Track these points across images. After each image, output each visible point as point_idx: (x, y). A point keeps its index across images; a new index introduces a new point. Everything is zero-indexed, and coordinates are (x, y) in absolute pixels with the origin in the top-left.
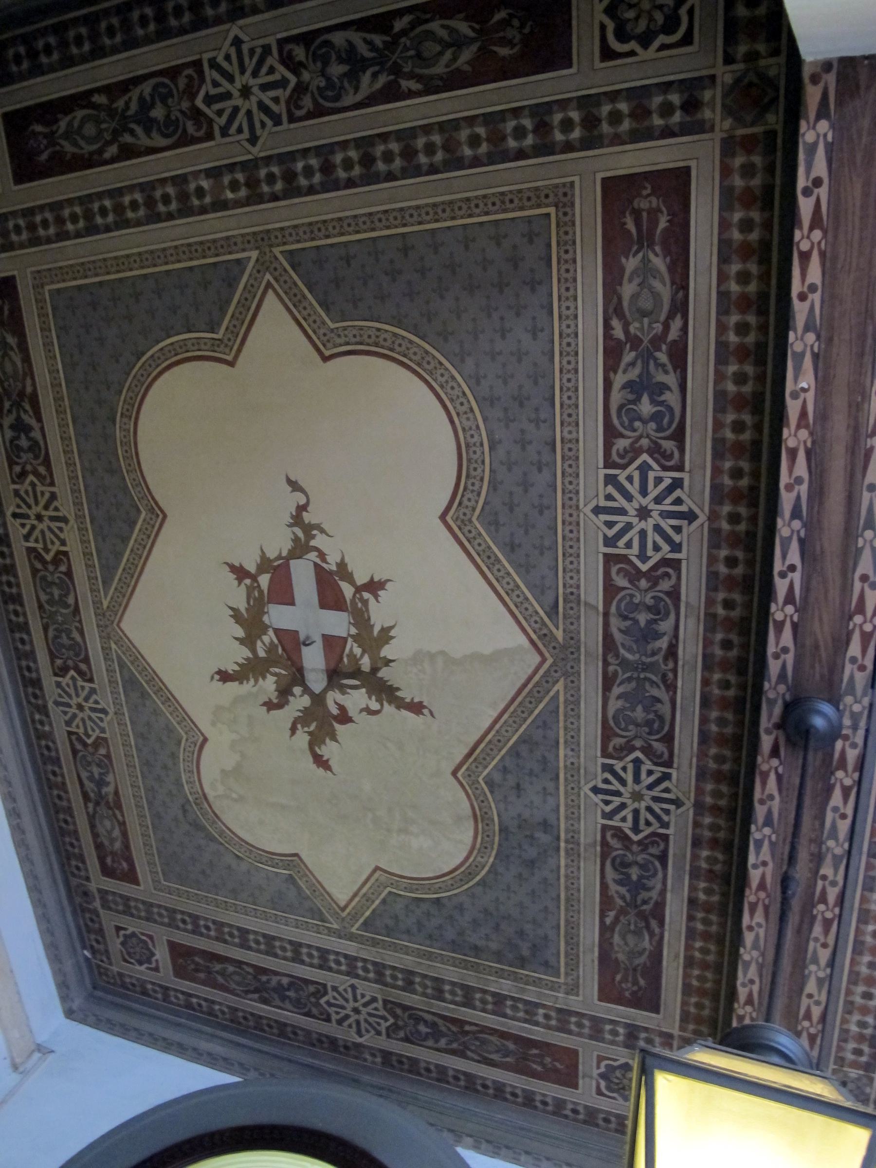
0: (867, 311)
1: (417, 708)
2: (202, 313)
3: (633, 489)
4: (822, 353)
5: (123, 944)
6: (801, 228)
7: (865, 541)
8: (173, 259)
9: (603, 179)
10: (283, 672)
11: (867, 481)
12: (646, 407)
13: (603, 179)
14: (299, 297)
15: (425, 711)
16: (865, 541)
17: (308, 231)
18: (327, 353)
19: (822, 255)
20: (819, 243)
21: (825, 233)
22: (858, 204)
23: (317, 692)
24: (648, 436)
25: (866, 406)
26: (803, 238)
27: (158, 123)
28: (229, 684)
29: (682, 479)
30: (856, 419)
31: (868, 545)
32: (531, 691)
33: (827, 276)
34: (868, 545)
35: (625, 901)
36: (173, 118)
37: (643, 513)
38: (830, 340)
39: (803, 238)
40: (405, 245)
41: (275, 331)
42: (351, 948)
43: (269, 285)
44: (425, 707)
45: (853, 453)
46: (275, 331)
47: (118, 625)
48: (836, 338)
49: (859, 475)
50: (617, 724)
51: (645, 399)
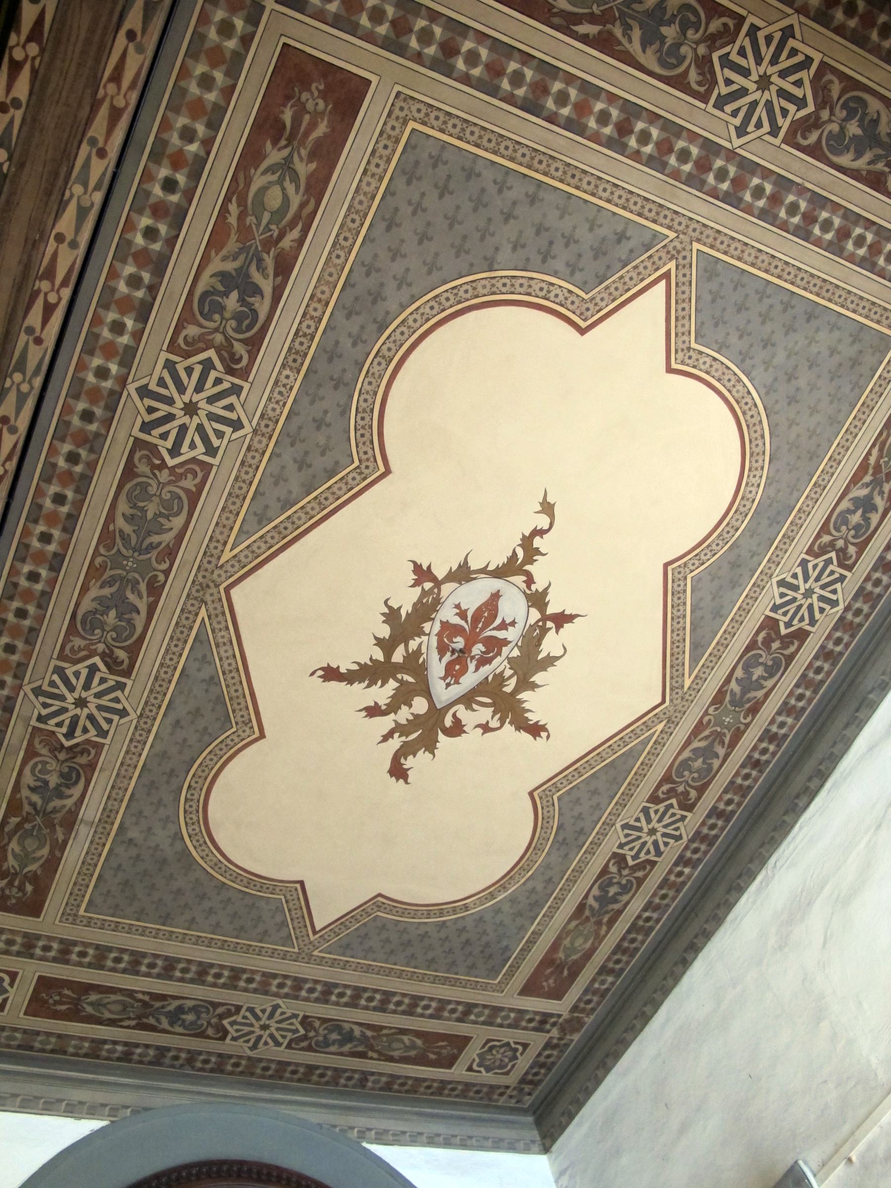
0: (65, 150)
1: (536, 730)
2: (582, 270)
3: (210, 390)
4: (10, 175)
5: (488, 1069)
6: (18, 33)
7: (13, 382)
8: (828, 287)
9: (369, 82)
10: (411, 679)
11: (25, 325)
12: (232, 302)
13: (369, 82)
14: (685, 296)
15: (544, 734)
16: (13, 382)
17: (442, 119)
18: (674, 366)
19: (34, 72)
20: (34, 59)
21: (42, 50)
22: (83, 35)
23: (439, 706)
24: (223, 333)
25: (42, 245)
26: (18, 45)
27: (861, 120)
28: (333, 684)
29: (242, 388)
30: (30, 256)
31: (15, 387)
32: (644, 721)
33: (34, 97)
34: (15, 387)
35: (35, 809)
36: (845, 113)
37: (191, 409)
38: (22, 165)
39: (18, 45)
40: (470, 170)
41: (642, 321)
42: (324, 974)
43: (667, 276)
44: (546, 730)
45: (19, 290)
46: (642, 321)
47: (663, 701)
48: (28, 164)
49: (20, 313)
50: (84, 622)
51: (234, 295)
